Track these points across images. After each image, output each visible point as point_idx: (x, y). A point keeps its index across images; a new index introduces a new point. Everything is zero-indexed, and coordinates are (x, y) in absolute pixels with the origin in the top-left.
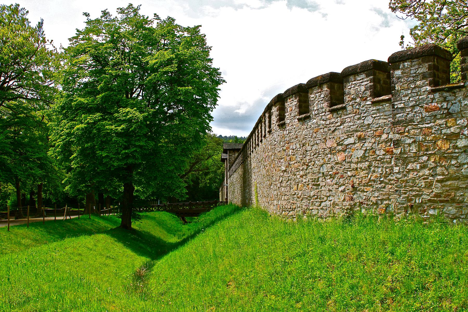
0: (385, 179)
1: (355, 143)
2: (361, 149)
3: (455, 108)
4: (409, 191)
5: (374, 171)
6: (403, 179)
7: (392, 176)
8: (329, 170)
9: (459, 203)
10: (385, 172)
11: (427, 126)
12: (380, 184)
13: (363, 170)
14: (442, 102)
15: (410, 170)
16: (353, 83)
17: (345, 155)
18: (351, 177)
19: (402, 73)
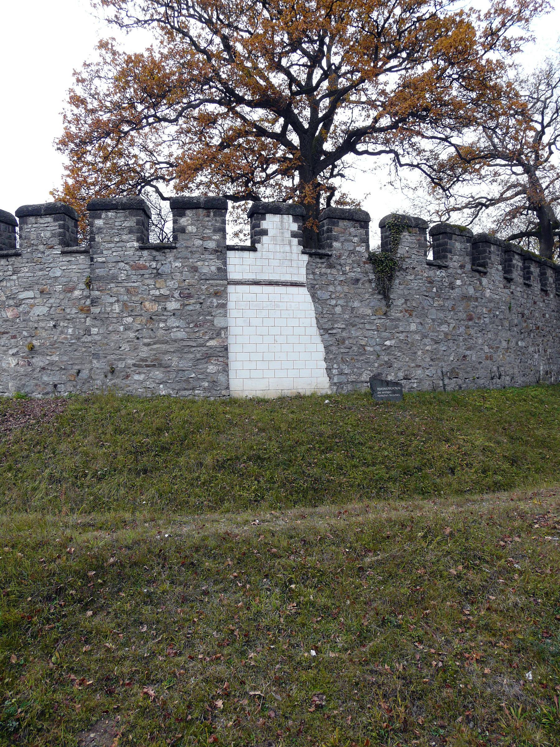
5: (62, 332)
19: (105, 223)
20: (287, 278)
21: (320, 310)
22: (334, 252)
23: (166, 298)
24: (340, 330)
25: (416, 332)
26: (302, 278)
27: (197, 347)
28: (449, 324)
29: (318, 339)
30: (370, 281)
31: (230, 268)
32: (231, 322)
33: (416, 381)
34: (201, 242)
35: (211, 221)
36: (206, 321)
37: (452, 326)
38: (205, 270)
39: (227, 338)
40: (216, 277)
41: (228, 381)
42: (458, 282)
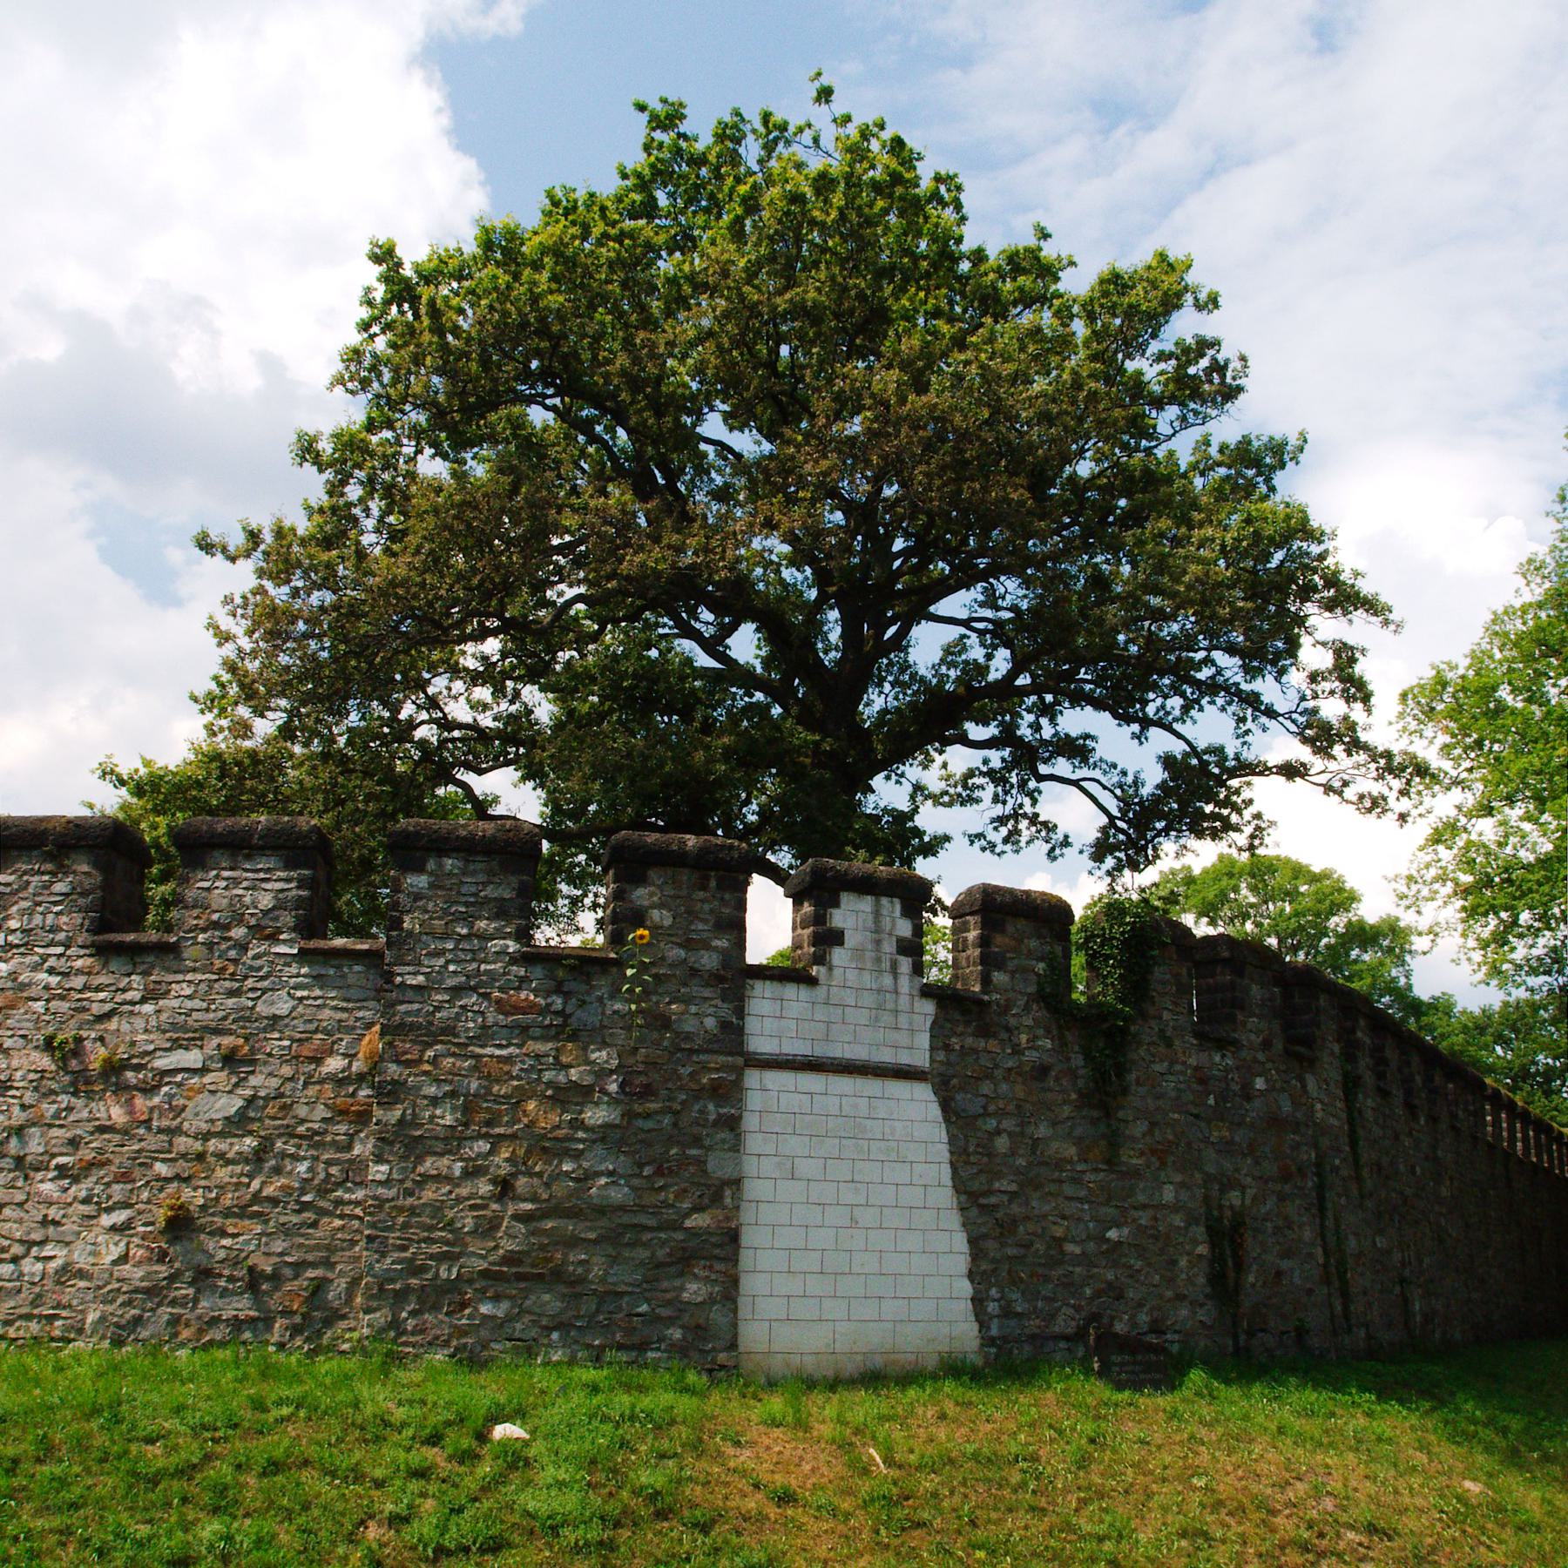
0: (320, 1197)
1: (204, 1071)
2: (230, 1092)
3: (581, 1016)
4: (418, 1242)
5: (277, 1171)
6: (400, 1203)
7: (349, 1190)
8: (55, 1150)
9: (572, 1284)
10: (322, 1176)
11: (498, 1052)
12: (299, 1212)
13: (229, 1162)
14: (548, 994)
15: (426, 1178)
16: (226, 874)
17: (150, 1104)
18: (168, 1180)
19: (432, 886)
20: (886, 1056)
21: (962, 1143)
22: (995, 996)
23: (583, 1094)
24: (1005, 1198)
25: (1175, 1208)
26: (919, 1055)
27: (659, 1229)
28: (1243, 1189)
29: (953, 1220)
30: (1072, 1074)
31: (752, 1025)
32: (750, 1166)
33: (1176, 1337)
34: (682, 953)
35: (707, 903)
36: (684, 1162)
37: (1250, 1192)
38: (689, 1026)
39: (738, 1208)
40: (716, 1046)
41: (735, 1325)
42: (1260, 1083)
